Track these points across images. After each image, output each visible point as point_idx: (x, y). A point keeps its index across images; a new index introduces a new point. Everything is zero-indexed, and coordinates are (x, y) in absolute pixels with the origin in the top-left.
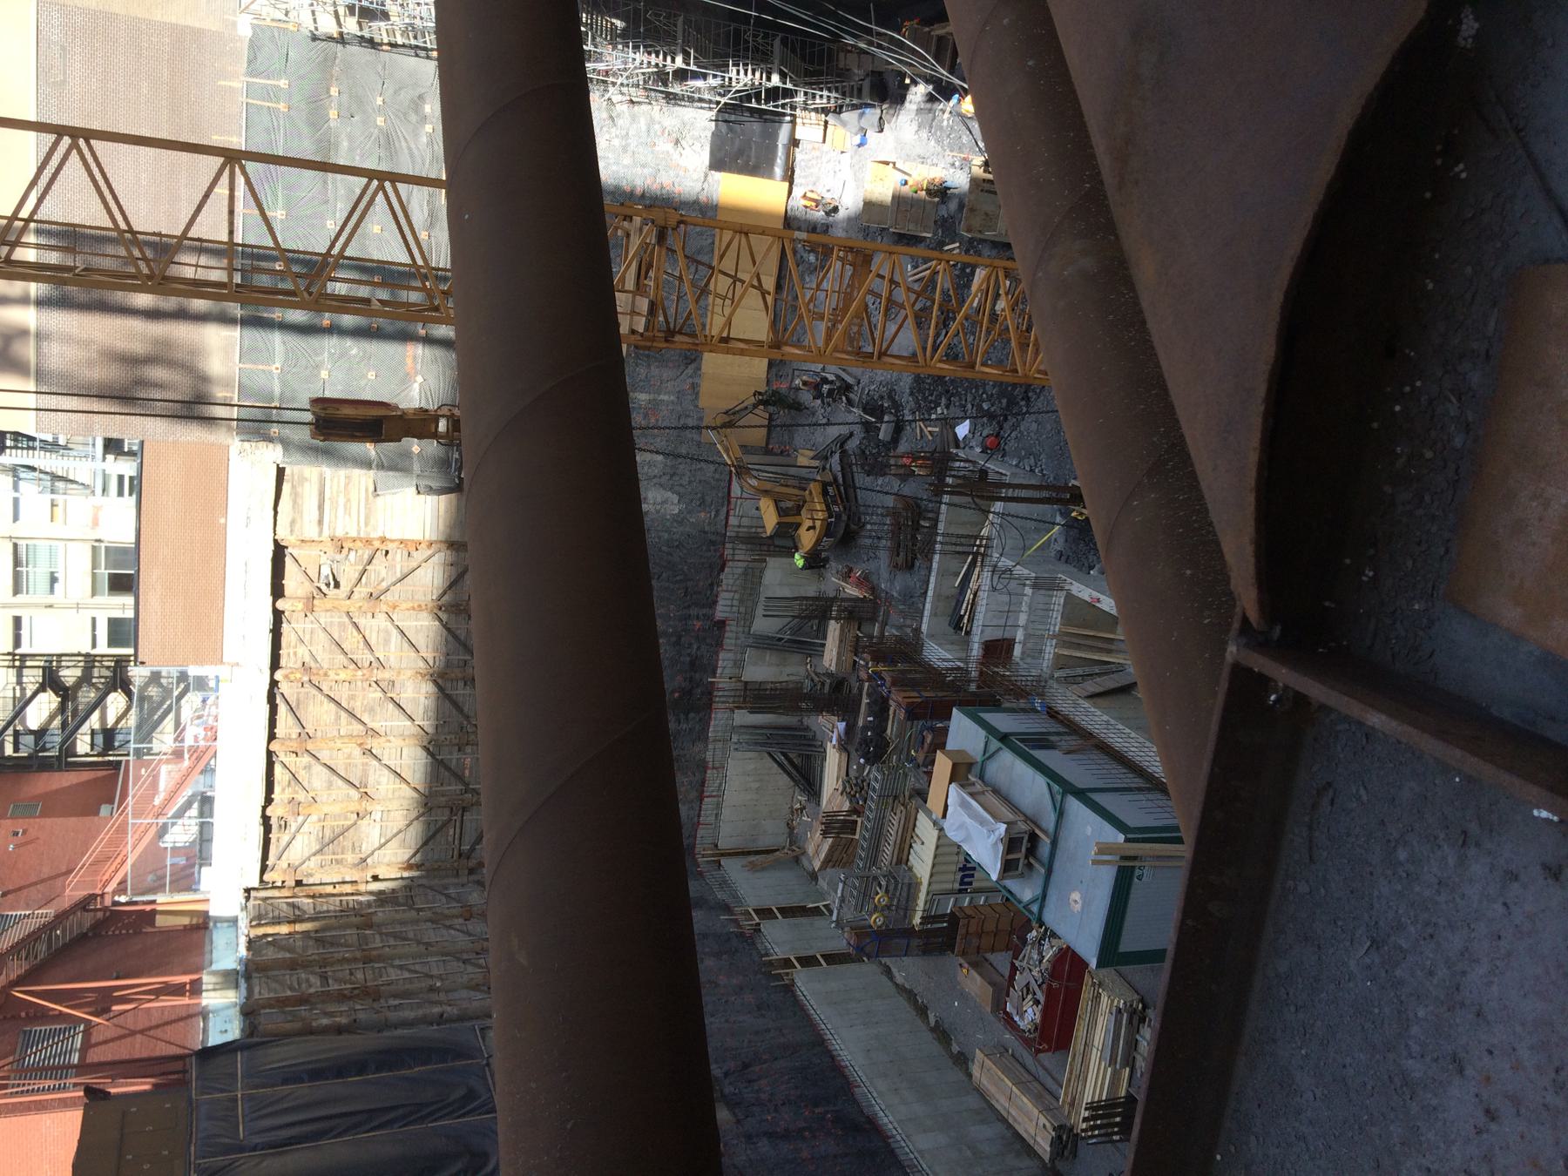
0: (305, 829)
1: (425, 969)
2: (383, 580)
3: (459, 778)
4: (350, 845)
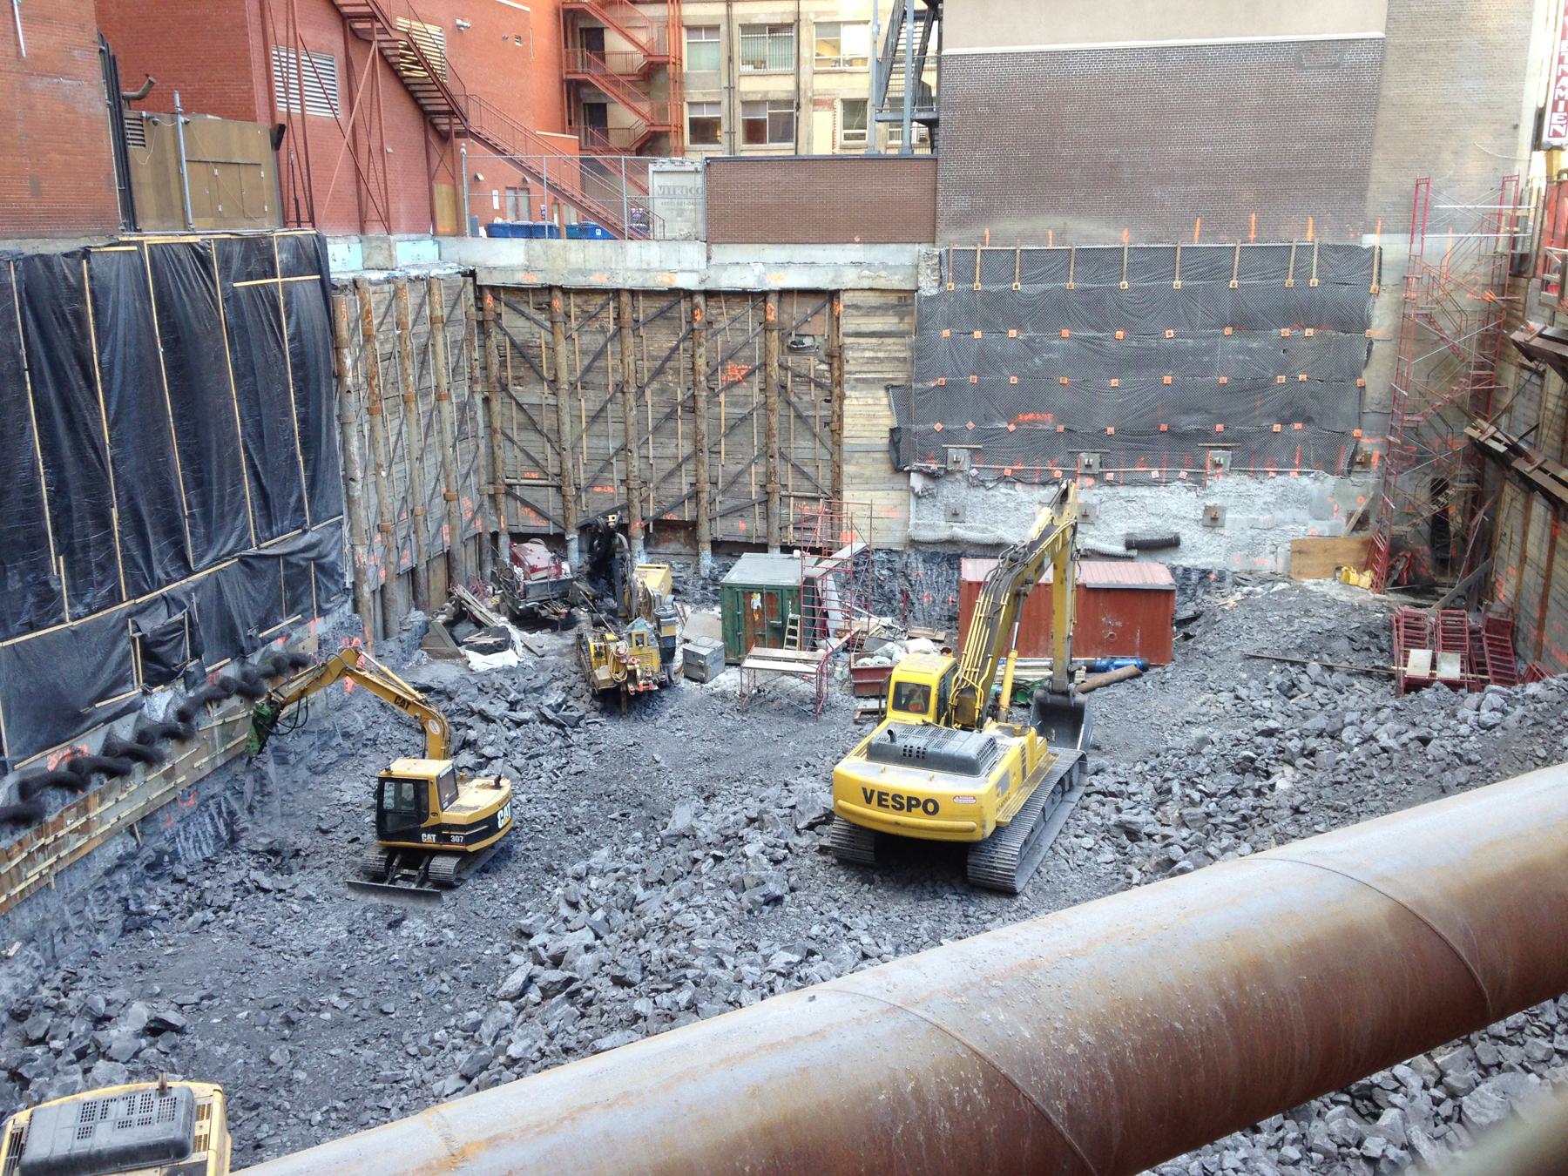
0: (536, 329)
1: (396, 460)
2: (800, 399)
3: (594, 481)
4: (521, 374)
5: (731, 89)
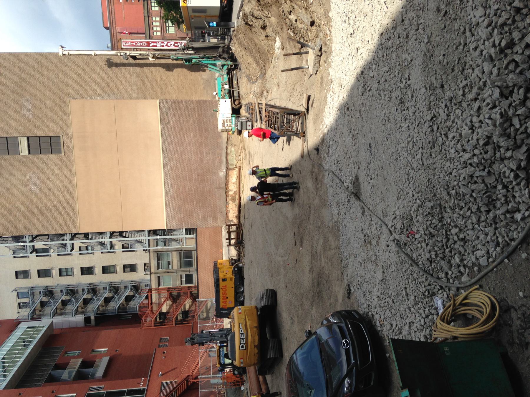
5: (176, 272)
